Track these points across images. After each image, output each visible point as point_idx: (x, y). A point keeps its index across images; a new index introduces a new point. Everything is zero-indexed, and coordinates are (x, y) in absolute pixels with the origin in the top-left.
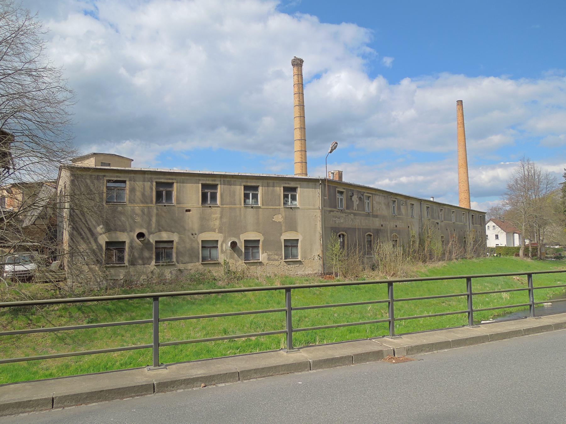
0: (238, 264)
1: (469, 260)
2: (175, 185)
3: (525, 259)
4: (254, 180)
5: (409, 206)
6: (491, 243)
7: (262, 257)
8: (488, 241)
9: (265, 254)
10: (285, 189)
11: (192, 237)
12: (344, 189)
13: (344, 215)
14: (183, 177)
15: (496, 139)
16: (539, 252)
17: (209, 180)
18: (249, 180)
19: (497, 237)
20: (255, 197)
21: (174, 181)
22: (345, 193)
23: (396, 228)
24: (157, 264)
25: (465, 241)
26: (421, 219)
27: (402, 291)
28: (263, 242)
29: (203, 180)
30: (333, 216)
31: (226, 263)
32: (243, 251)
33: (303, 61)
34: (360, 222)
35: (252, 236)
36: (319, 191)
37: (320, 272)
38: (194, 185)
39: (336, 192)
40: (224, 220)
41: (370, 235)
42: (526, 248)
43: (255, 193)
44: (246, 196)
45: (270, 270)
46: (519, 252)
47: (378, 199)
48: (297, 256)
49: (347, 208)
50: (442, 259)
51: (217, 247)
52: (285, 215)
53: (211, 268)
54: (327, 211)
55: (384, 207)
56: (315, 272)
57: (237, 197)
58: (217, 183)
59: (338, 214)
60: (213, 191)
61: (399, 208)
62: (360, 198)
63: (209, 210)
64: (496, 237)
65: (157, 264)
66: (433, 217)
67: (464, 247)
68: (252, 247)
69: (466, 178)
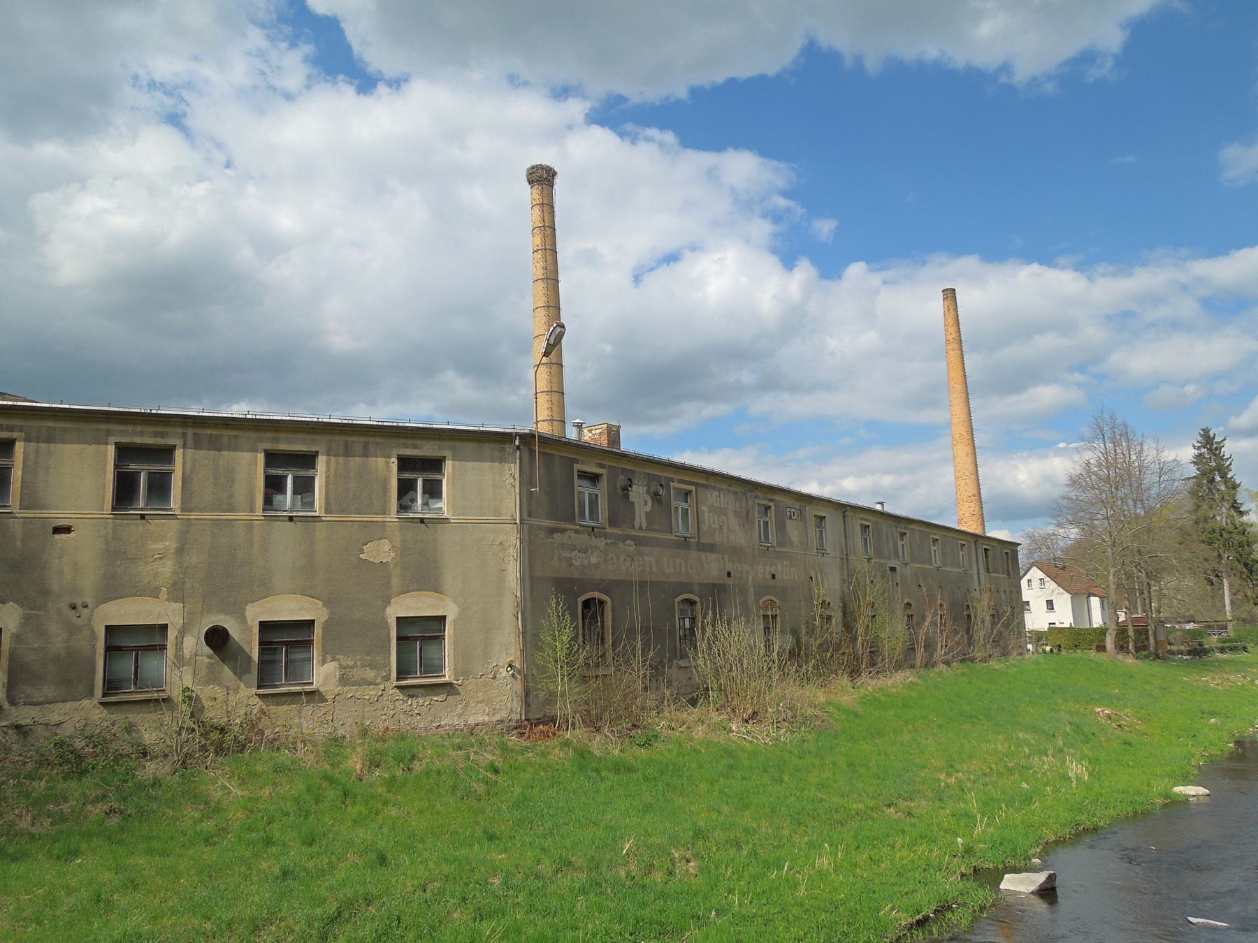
0: (235, 699)
1: (979, 666)
2: (19, 447)
3: (1120, 657)
4: (300, 436)
5: (812, 523)
6: (1037, 620)
8: (1027, 616)
9: (331, 667)
10: (405, 464)
11: (72, 613)
12: (601, 466)
13: (600, 543)
14: (51, 424)
15: (1046, 395)
16: (1151, 639)
17: (142, 434)
18: (282, 435)
19: (1050, 604)
20: (304, 487)
21: (15, 435)
22: (605, 479)
23: (772, 582)
24: (261, 691)
25: (969, 616)
26: (845, 559)
27: (765, 771)
29: (122, 433)
30: (563, 546)
31: (189, 697)
32: (255, 655)
33: (555, 174)
34: (660, 565)
35: (287, 609)
36: (511, 470)
37: (515, 717)
38: (90, 449)
39: (571, 477)
40: (192, 559)
41: (692, 603)
42: (1122, 631)
43: (303, 473)
44: (274, 485)
45: (345, 721)
46: (1103, 641)
47: (713, 498)
48: (441, 668)
49: (613, 522)
50: (905, 661)
51: (163, 647)
53: (134, 716)
54: (540, 528)
55: (734, 522)
56: (498, 717)
58: (171, 442)
59: (584, 538)
60: (157, 468)
61: (781, 527)
62: (656, 494)
63: (138, 528)
64: (1046, 606)
65: (261, 691)
66: (879, 553)
67: (968, 633)
68: (287, 644)
69: (971, 467)
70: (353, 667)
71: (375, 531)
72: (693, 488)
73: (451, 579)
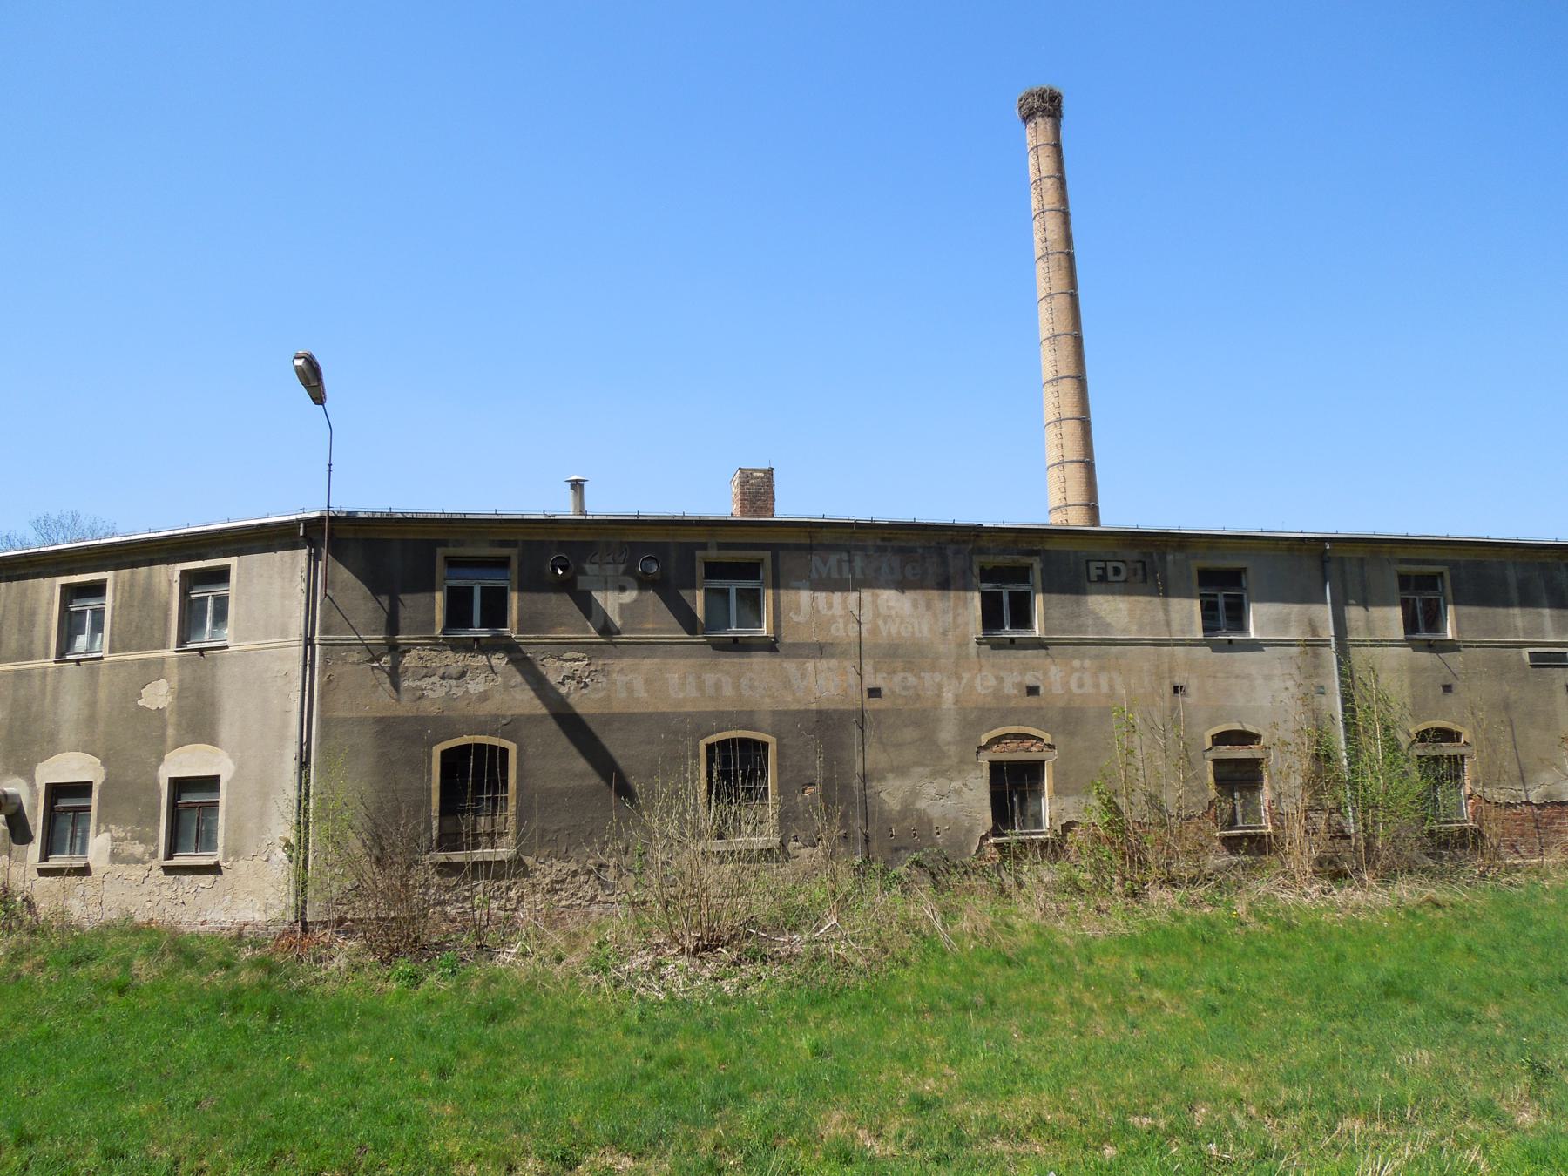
7: (98, 846)
28: (104, 787)
52: (181, 681)
57: (39, 632)
70: (125, 839)
71: (150, 671)
72: (767, 555)
73: (227, 729)
